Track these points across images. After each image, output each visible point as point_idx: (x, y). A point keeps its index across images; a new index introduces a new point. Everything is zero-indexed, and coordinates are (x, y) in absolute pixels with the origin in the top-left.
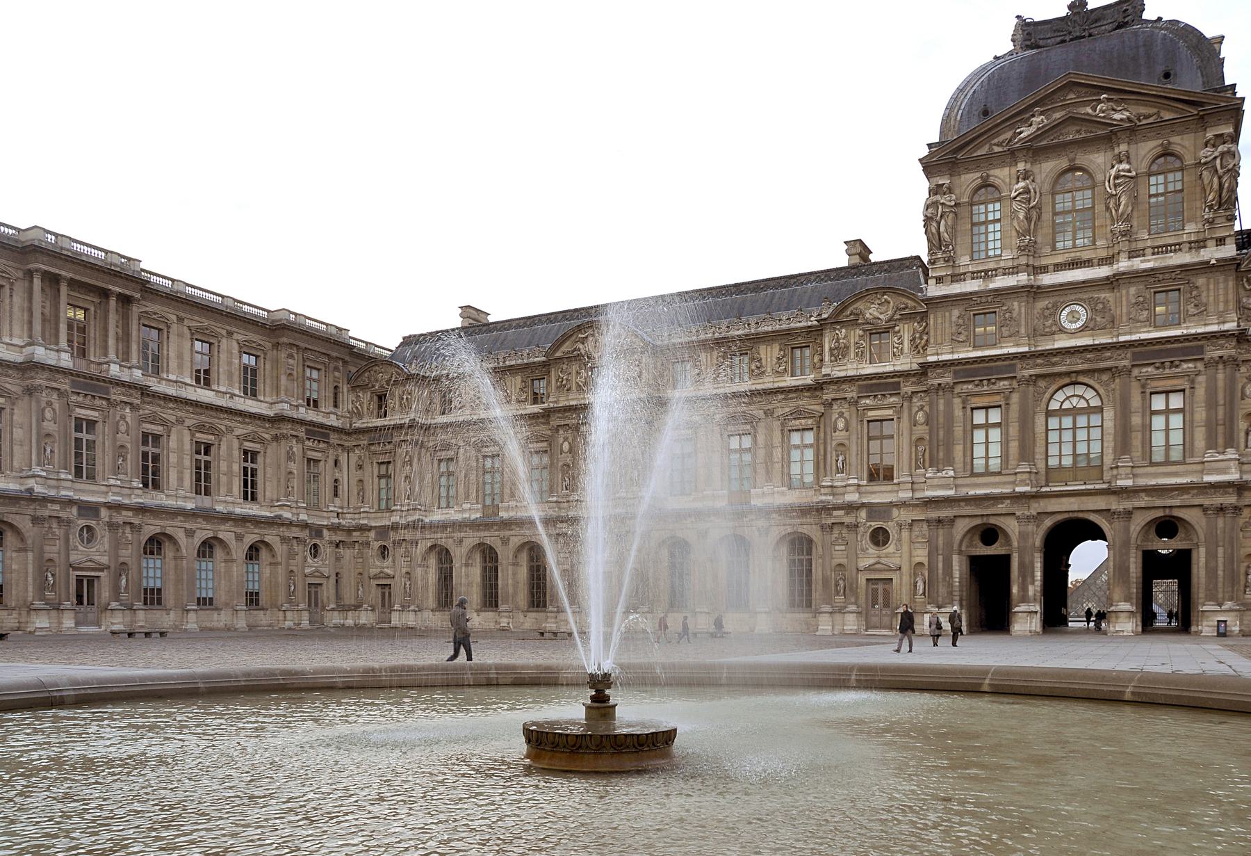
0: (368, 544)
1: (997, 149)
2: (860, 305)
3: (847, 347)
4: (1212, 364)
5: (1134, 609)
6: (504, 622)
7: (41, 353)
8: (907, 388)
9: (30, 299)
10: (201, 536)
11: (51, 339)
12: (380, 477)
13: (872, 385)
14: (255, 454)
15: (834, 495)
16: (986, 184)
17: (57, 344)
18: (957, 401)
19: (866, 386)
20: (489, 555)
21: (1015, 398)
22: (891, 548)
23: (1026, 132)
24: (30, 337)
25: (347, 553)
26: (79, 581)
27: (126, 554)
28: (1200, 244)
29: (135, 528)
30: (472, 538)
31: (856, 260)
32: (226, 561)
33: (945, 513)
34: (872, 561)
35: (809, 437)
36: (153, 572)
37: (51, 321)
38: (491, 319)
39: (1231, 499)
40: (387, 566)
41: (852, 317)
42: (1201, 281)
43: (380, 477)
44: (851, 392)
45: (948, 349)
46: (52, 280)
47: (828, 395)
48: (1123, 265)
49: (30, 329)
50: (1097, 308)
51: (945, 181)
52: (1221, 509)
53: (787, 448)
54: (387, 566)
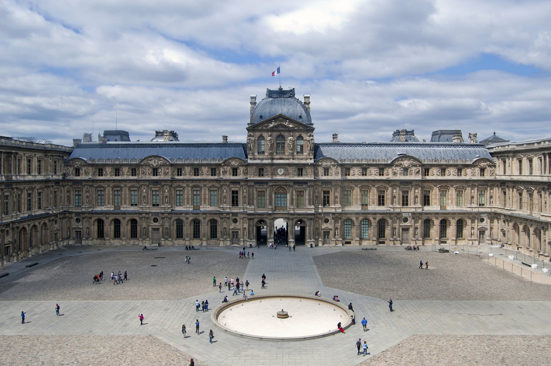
0: (72, 218)
1: (264, 128)
2: (230, 161)
4: (309, 186)
6: (124, 243)
8: (242, 184)
12: (76, 195)
16: (261, 136)
18: (255, 189)
20: (117, 222)
21: (268, 190)
22: (238, 224)
23: (271, 126)
25: (64, 221)
28: (307, 159)
30: (112, 217)
32: (35, 231)
33: (252, 217)
39: (313, 217)
40: (80, 225)
42: (307, 168)
47: (222, 184)
48: (291, 161)
50: (286, 170)
51: (252, 134)
52: (311, 219)
54: (80, 225)
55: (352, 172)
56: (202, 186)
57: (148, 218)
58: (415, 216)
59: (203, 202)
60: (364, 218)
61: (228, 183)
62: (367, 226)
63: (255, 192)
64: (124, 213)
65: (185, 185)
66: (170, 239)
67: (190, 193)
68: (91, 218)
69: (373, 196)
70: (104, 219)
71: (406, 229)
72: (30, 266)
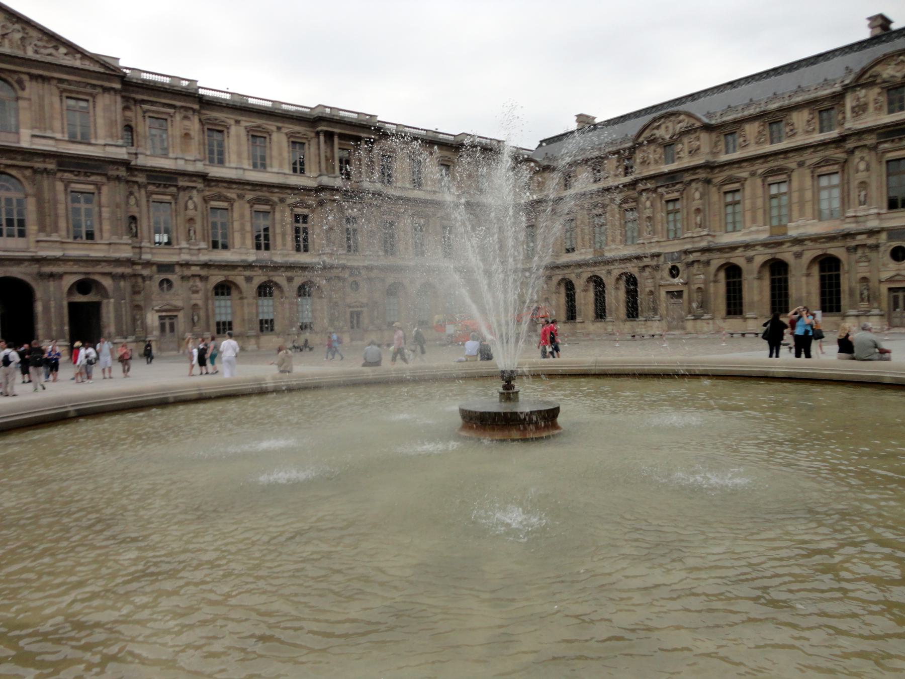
2: (878, 69)
3: (866, 104)
7: (326, 180)
9: (319, 149)
10: (257, 281)
11: (330, 170)
12: (669, 213)
13: (890, 132)
14: (305, 217)
15: (857, 222)
17: (334, 173)
19: (884, 133)
20: (598, 282)
24: (320, 171)
26: (352, 313)
27: (198, 299)
29: (204, 279)
30: (587, 273)
31: (878, 31)
34: (892, 274)
35: (835, 180)
36: (223, 309)
37: (329, 159)
38: (597, 121)
41: (871, 79)
43: (669, 213)
44: (870, 140)
46: (329, 136)
47: (850, 145)
49: (320, 166)
53: (817, 190)
56: (793, 165)
57: (657, 268)
59: (795, 213)
63: (61, 196)
65: (745, 175)
66: (706, 316)
67: (760, 191)
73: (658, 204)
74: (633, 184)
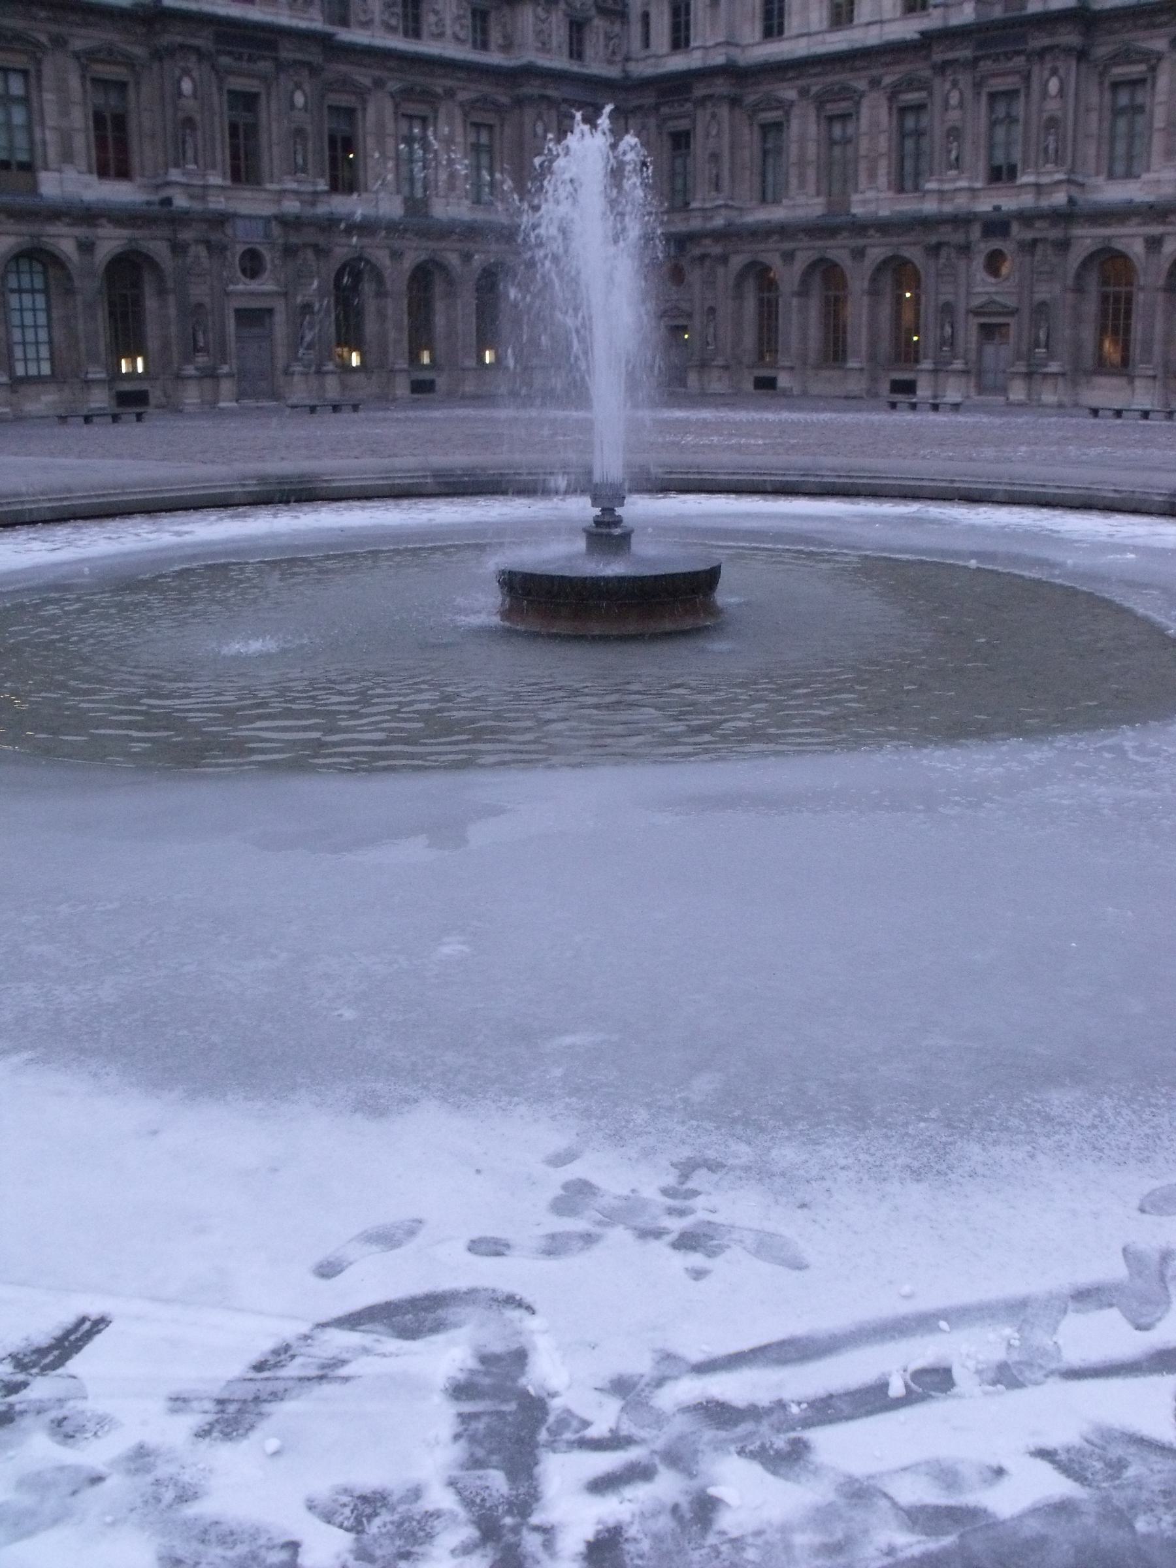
5: (864, 365)
12: (1117, 112)
29: (320, 252)
43: (1117, 112)
45: (287, 12)
55: (432, 18)
58: (301, 236)
60: (25, 242)
61: (203, 41)
62: (40, 300)
64: (860, 227)
68: (724, 259)
69: (65, 113)
70: (774, 260)
71: (253, 318)
72: (1127, 469)
73: (1093, 97)
74: (928, 39)
